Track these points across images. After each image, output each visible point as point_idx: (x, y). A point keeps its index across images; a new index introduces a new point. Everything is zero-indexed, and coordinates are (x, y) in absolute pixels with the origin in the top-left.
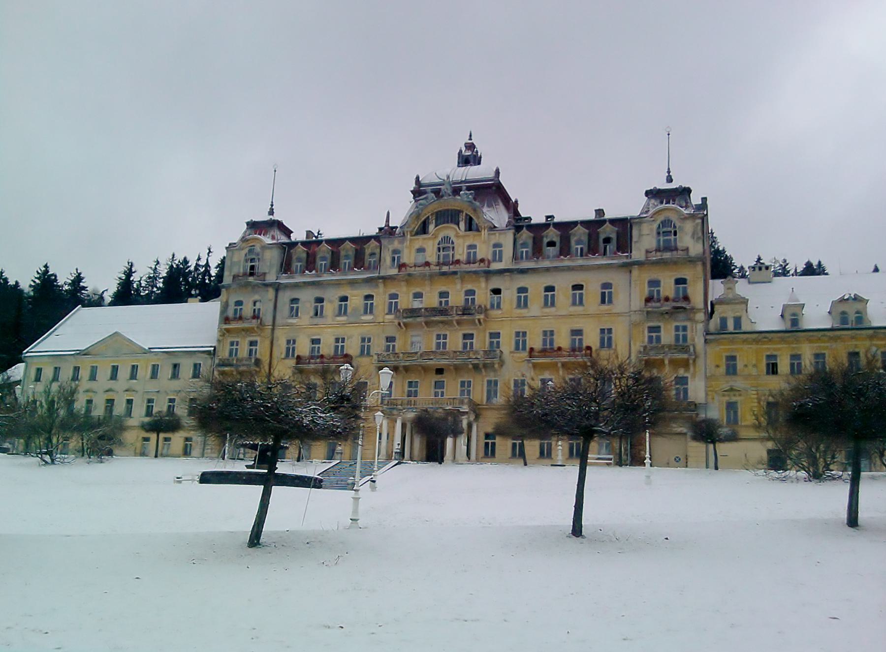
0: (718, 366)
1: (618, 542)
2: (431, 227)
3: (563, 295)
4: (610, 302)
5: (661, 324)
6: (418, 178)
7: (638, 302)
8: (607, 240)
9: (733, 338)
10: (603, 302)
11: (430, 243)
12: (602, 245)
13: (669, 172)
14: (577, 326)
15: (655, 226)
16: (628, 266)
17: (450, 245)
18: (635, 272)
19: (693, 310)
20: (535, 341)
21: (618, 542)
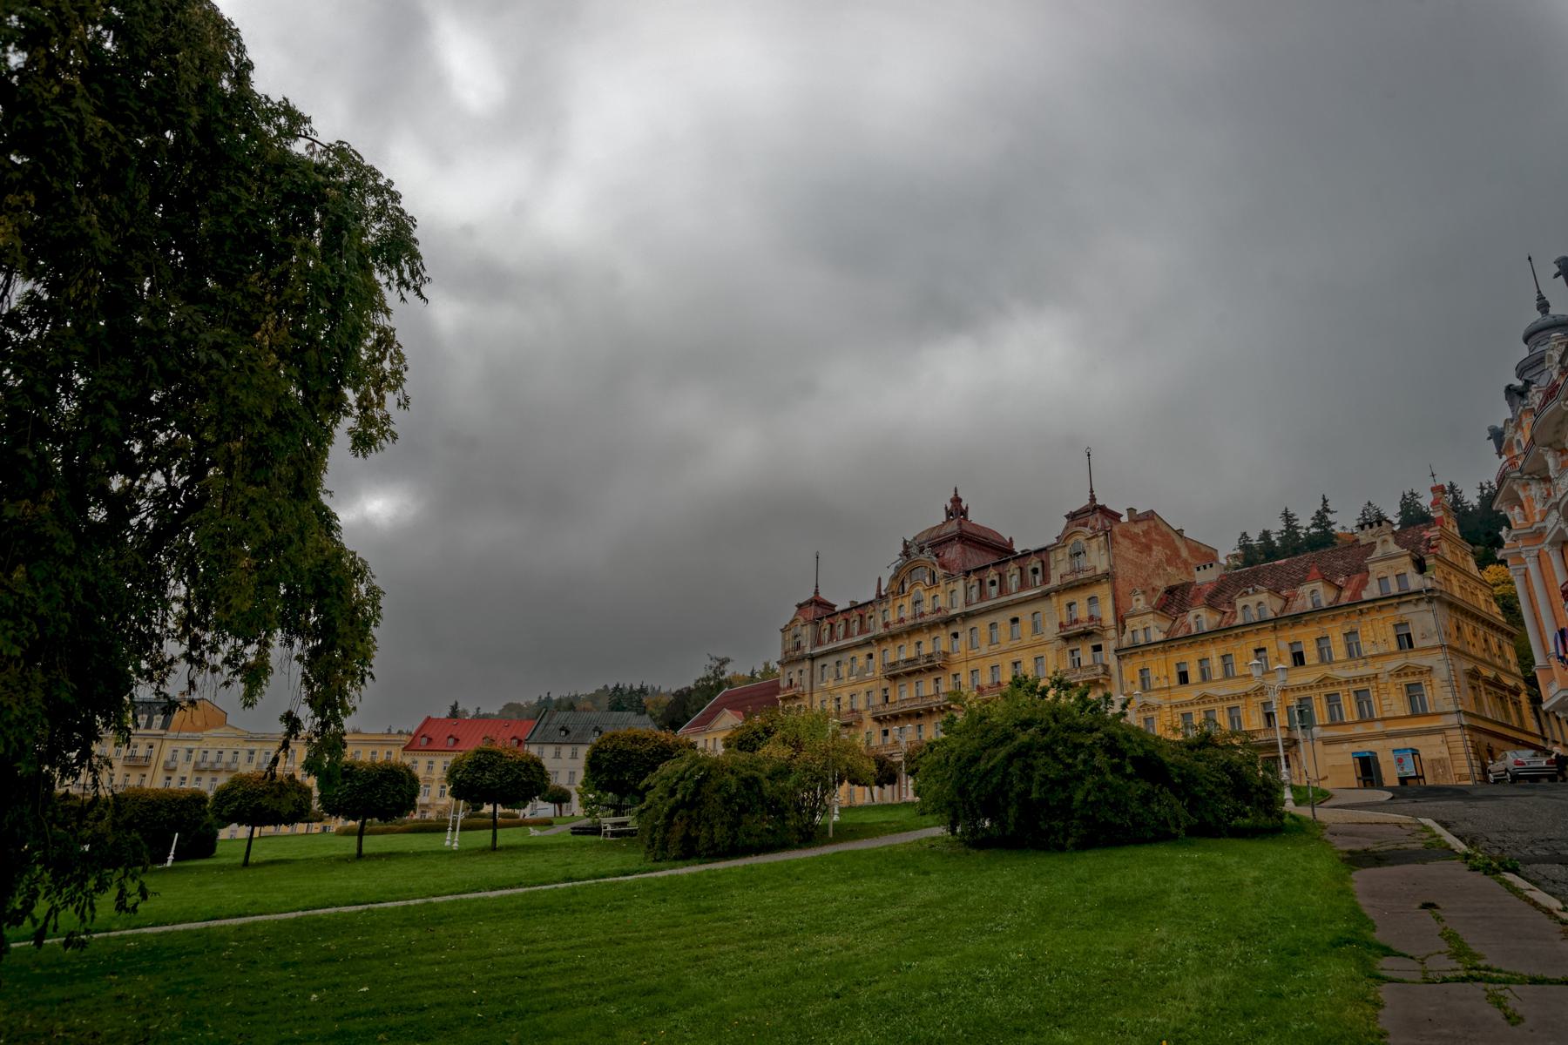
16: (1046, 595)
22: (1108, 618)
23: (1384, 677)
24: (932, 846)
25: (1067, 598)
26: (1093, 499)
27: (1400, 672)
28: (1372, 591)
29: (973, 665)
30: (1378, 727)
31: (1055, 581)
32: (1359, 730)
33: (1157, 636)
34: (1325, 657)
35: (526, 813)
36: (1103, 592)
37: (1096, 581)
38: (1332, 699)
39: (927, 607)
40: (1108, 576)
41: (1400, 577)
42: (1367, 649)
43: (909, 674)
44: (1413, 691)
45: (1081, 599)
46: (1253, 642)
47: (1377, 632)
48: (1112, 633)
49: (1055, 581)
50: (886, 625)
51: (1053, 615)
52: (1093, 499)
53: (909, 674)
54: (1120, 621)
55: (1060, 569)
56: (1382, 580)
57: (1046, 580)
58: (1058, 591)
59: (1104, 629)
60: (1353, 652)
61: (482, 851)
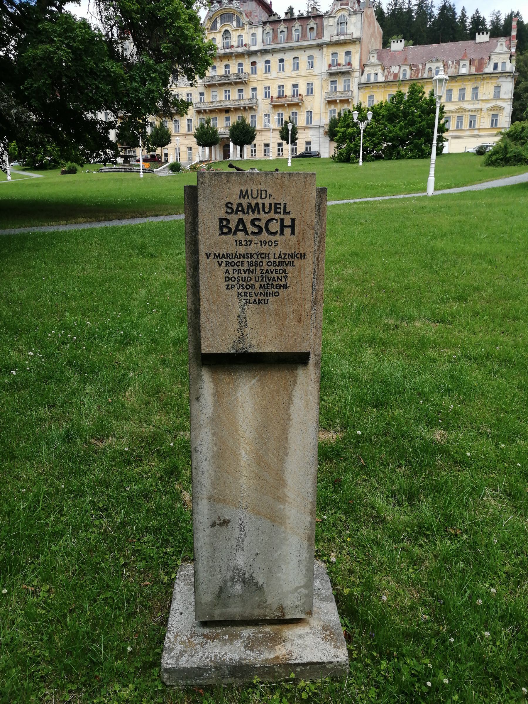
2: (219, 25)
7: (325, 68)
11: (218, 35)
15: (336, 19)
16: (320, 46)
18: (325, 49)
19: (353, 71)
22: (356, 64)
23: (484, 110)
27: (492, 109)
28: (489, 69)
30: (476, 132)
32: (468, 133)
33: (381, 78)
34: (462, 98)
36: (354, 49)
37: (353, 42)
38: (460, 118)
39: (234, 40)
41: (504, 63)
42: (480, 97)
43: (221, 85)
44: (495, 116)
45: (341, 52)
47: (487, 90)
48: (357, 74)
49: (326, 38)
50: (227, 119)
51: (323, 61)
53: (221, 85)
54: (363, 67)
56: (369, 75)
57: (320, 35)
58: (329, 44)
59: (353, 71)
60: (475, 96)
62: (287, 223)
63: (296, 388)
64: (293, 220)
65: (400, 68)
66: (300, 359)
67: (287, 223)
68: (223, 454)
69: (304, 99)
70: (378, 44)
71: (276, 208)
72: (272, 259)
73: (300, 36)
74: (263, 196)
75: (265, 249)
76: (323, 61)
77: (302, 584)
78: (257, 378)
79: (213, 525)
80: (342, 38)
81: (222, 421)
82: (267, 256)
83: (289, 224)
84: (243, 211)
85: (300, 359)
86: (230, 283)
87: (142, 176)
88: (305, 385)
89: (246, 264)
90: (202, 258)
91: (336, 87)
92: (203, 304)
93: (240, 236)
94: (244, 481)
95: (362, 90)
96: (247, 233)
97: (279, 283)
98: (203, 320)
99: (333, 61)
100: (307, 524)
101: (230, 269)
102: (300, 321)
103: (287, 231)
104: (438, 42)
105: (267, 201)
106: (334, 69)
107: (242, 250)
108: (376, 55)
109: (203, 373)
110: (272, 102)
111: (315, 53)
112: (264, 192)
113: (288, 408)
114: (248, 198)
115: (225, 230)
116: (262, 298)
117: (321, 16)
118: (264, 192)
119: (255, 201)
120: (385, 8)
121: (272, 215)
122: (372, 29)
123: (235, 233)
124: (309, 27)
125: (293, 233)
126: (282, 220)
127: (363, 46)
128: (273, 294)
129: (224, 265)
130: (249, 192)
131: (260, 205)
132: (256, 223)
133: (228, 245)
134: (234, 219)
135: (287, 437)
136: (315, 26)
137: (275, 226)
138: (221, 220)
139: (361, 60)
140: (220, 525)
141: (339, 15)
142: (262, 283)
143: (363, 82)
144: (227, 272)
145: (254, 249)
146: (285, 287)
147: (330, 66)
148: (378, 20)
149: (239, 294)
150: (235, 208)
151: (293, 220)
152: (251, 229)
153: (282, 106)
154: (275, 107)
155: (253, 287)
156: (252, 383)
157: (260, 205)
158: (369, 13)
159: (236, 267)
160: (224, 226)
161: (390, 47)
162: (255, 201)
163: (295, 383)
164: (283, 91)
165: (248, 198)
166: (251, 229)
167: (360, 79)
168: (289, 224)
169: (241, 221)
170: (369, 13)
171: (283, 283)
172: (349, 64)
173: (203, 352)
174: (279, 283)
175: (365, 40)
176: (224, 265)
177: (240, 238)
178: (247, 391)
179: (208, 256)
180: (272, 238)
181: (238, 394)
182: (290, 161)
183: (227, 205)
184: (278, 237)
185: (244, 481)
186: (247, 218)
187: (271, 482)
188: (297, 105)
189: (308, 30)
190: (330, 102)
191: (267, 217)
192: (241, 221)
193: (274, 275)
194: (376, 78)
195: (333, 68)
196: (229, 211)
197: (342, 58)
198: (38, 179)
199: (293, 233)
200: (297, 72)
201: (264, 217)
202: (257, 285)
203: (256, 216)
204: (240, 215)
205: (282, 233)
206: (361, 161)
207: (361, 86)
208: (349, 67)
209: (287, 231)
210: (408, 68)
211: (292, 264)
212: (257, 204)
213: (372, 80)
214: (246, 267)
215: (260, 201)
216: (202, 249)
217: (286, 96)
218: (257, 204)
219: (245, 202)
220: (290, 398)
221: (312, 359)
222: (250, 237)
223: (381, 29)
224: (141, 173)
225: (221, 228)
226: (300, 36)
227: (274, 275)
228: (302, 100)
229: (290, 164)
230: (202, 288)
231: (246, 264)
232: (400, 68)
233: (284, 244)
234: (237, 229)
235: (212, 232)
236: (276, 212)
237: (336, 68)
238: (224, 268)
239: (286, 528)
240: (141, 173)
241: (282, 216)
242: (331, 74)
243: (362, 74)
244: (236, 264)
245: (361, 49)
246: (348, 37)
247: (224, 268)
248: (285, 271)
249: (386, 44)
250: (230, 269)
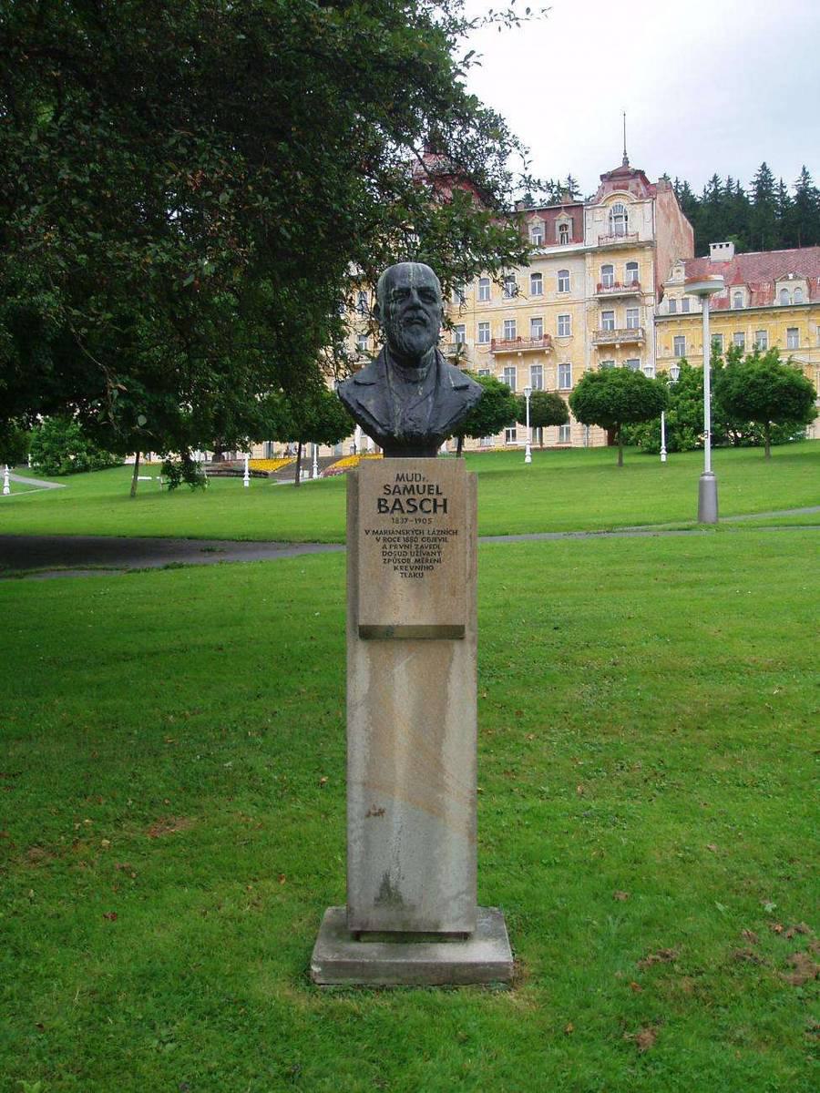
0: (667, 348)
1: (627, 466)
3: (718, 247)
4: (567, 289)
5: (614, 310)
6: (764, 163)
7: (591, 291)
8: (563, 227)
9: (722, 308)
10: (561, 290)
12: (558, 233)
13: (625, 154)
14: (535, 316)
15: (607, 211)
16: (580, 255)
17: (623, 214)
18: (589, 260)
19: (644, 295)
20: (498, 333)
21: (627, 466)
22: (649, 287)
24: (292, 485)
25: (606, 260)
26: (626, 162)
29: (481, 318)
31: (591, 241)
35: (374, 299)
37: (640, 247)
40: (651, 244)
45: (619, 264)
46: (787, 322)
48: (651, 300)
49: (591, 241)
51: (585, 280)
52: (626, 162)
55: (597, 228)
57: (579, 237)
58: (594, 252)
59: (644, 295)
61: (609, 467)
62: (440, 502)
63: (453, 665)
64: (445, 500)
65: (729, 292)
66: (453, 633)
67: (440, 502)
68: (377, 736)
69: (553, 343)
70: (688, 252)
71: (429, 489)
72: (426, 536)
73: (543, 239)
74: (418, 479)
75: (420, 526)
76: (585, 280)
77: (464, 888)
78: (414, 654)
79: (368, 815)
80: (620, 240)
81: (378, 700)
82: (421, 532)
83: (442, 504)
84: (399, 492)
85: (453, 633)
86: (387, 557)
87: (246, 484)
88: (463, 659)
89: (402, 540)
90: (362, 534)
91: (612, 323)
92: (362, 578)
93: (397, 514)
94: (400, 768)
95: (662, 327)
96: (403, 512)
97: (434, 557)
98: (361, 593)
99: (605, 279)
100: (467, 817)
101: (388, 545)
102: (454, 594)
103: (440, 510)
104: (795, 246)
105: (421, 484)
106: (607, 293)
107: (397, 527)
108: (683, 269)
109: (359, 647)
110: (493, 348)
111: (572, 266)
112: (418, 476)
113: (445, 687)
114: (414, 493)
115: (383, 509)
116: (418, 571)
117: (580, 207)
118: (418, 476)
119: (410, 483)
120: (698, 192)
121: (426, 496)
122: (672, 225)
123: (392, 512)
124: (558, 224)
125: (445, 511)
126: (435, 500)
127: (659, 252)
128: (428, 568)
129: (381, 540)
130: (405, 476)
131: (415, 487)
132: (412, 502)
133: (386, 522)
134: (391, 499)
135: (444, 718)
136: (569, 223)
137: (428, 506)
138: (379, 500)
139: (656, 277)
140: (375, 815)
141: (612, 204)
142: (417, 558)
143: (662, 313)
144: (384, 547)
145: (411, 526)
146: (439, 561)
147: (599, 287)
148: (684, 210)
149: (395, 568)
150: (392, 490)
151: (445, 500)
152: (406, 507)
153: (512, 356)
154: (498, 357)
155: (408, 560)
156: (408, 659)
157: (415, 487)
158: (665, 200)
159: (392, 543)
160: (381, 504)
161: (708, 253)
162: (410, 483)
163: (451, 660)
164: (514, 330)
165: (414, 493)
166: (406, 507)
167: (657, 309)
168: (442, 504)
169: (397, 501)
170: (665, 200)
171: (437, 557)
172: (635, 283)
173: (361, 624)
174: (434, 557)
175: (662, 243)
176: (381, 540)
177: (397, 516)
178: (404, 674)
179: (367, 533)
180: (426, 516)
181: (396, 670)
182: (528, 453)
183: (385, 487)
184: (431, 515)
185: (400, 768)
186: (403, 499)
187: (430, 767)
188: (540, 353)
189: (557, 228)
190: (602, 349)
191: (422, 497)
192: (397, 501)
193: (428, 550)
194: (686, 306)
195: (605, 291)
196: (388, 492)
197: (621, 273)
198: (57, 489)
199: (445, 511)
200: (541, 297)
201: (419, 497)
202: (413, 560)
203: (411, 496)
204: (397, 496)
205: (435, 511)
206: (663, 451)
207: (659, 320)
208: (636, 288)
209: (440, 510)
210: (743, 289)
211: (445, 540)
212: (412, 486)
213: (680, 312)
214: (402, 542)
215: (415, 484)
216: (362, 525)
217: (519, 338)
218: (412, 486)
219: (401, 484)
220: (447, 673)
221: (468, 634)
222: (406, 515)
223: (689, 225)
224: (246, 478)
225: (380, 506)
226: (543, 239)
227: (428, 550)
228: (550, 345)
229: (528, 459)
230: (361, 561)
231: (402, 540)
232: (729, 292)
233: (438, 521)
234: (394, 508)
235: (371, 510)
236: (429, 493)
237: (612, 290)
238: (381, 543)
239: (445, 821)
240: (246, 478)
241: (435, 496)
242: (602, 301)
243: (661, 301)
244: (393, 539)
245: (655, 258)
246: (630, 240)
247: (381, 543)
248: (438, 547)
249: (701, 250)
250: (388, 545)
